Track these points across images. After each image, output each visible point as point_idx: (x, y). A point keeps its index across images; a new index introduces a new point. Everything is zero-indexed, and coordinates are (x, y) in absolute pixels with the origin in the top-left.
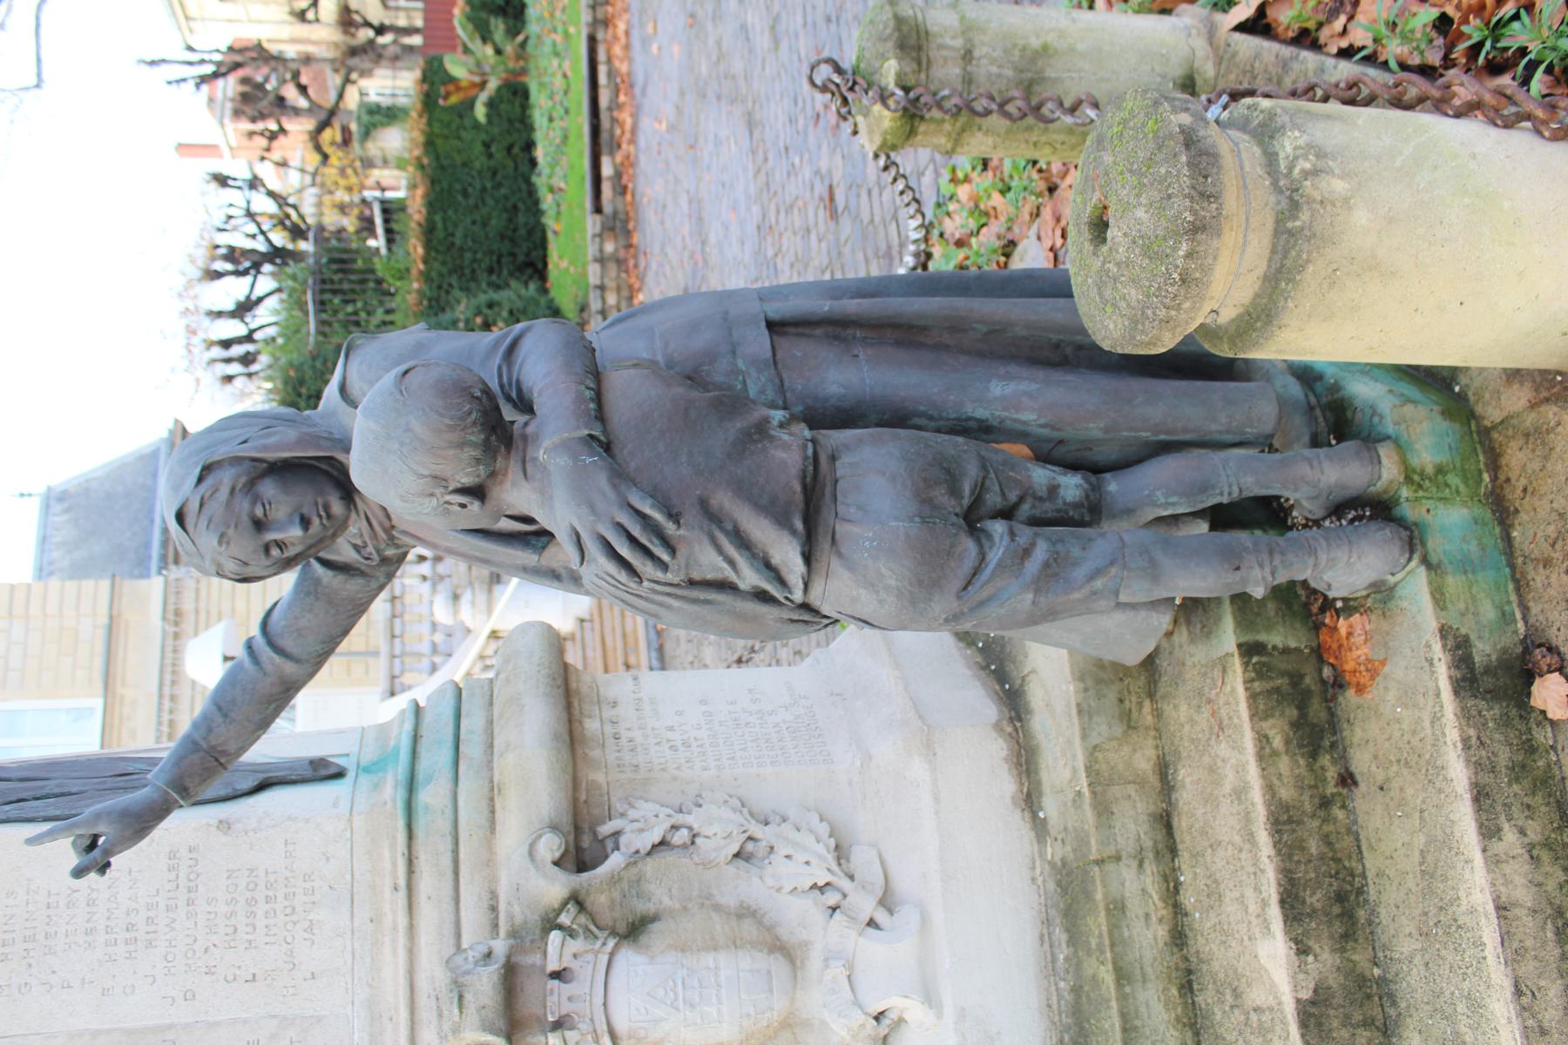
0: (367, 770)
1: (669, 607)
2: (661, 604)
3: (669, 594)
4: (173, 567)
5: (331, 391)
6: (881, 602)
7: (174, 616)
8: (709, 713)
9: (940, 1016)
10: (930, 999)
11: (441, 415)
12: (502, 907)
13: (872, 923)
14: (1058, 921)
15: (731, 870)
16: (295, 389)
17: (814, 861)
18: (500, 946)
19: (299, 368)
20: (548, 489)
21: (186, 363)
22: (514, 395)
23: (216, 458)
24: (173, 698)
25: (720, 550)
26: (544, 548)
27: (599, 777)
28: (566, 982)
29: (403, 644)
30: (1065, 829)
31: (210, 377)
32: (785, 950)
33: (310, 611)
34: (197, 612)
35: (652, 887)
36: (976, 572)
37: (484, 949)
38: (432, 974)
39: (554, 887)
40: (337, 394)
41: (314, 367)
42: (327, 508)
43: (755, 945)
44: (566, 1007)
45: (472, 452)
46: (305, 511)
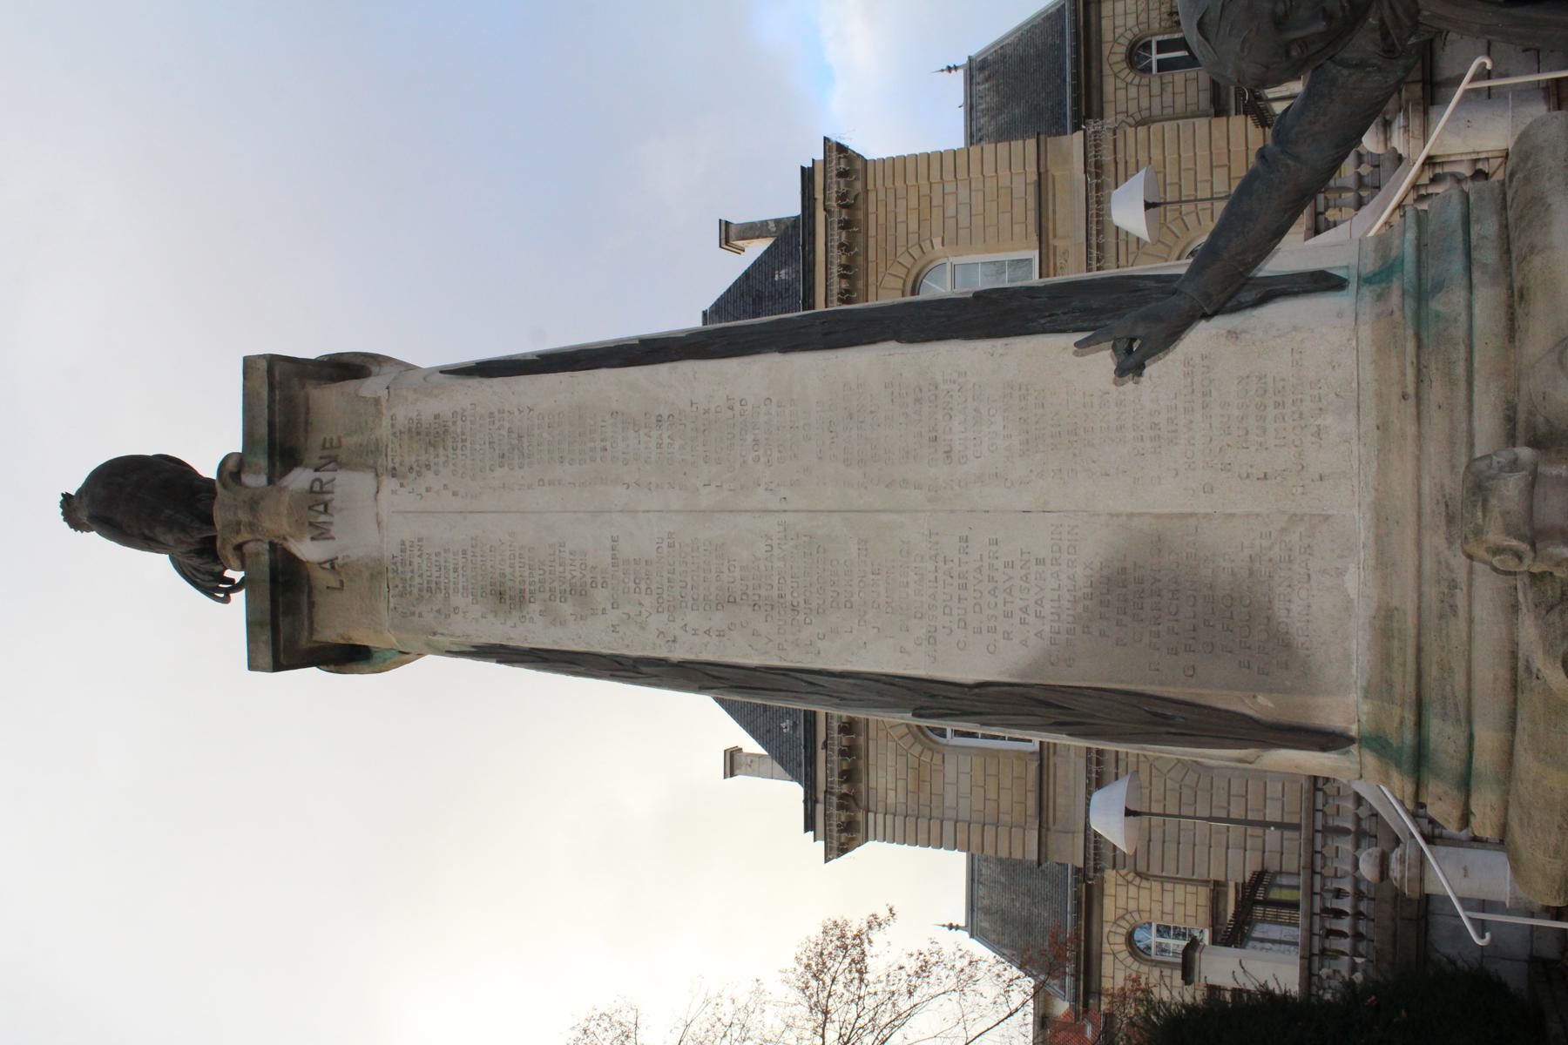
7: (1094, 168)
24: (1100, 247)
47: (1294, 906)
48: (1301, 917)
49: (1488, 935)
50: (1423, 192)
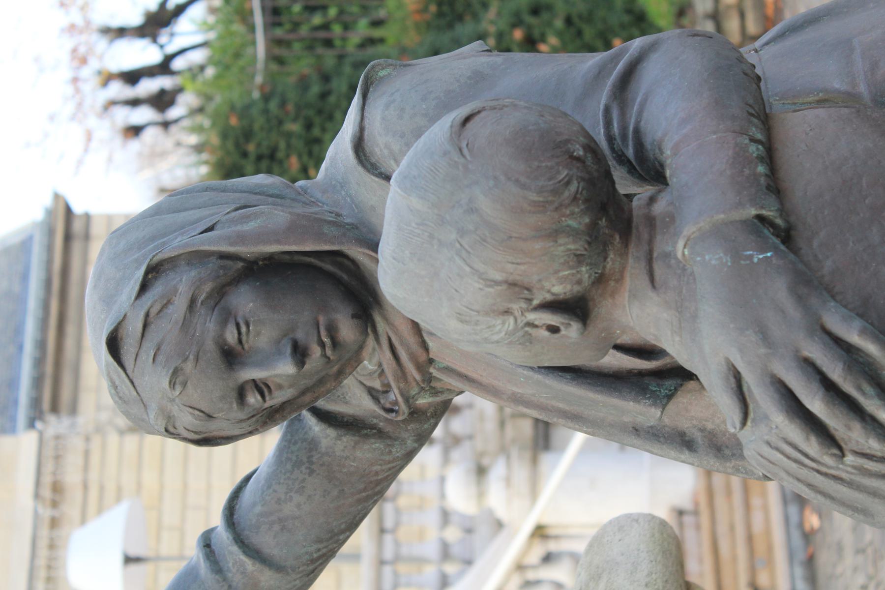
4: (51, 419)
5: (340, 148)
7: (52, 493)
11: (523, 187)
16: (237, 145)
19: (244, 112)
20: (694, 307)
21: (70, 107)
22: (630, 153)
23: (166, 254)
26: (669, 397)
29: (397, 544)
31: (106, 129)
33: (301, 490)
34: (85, 487)
40: (350, 153)
41: (266, 111)
42: (332, 330)
45: (568, 245)
46: (300, 335)
50: (531, 575)
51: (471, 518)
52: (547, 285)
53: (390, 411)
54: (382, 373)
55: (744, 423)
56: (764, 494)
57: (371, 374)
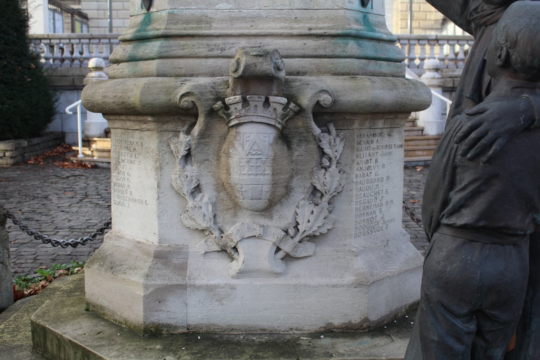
0: (365, 17)
1: (443, 157)
2: (445, 153)
3: (449, 157)
6: (438, 263)
8: (382, 179)
9: (233, 277)
10: (241, 274)
12: (299, 77)
13: (278, 249)
14: (271, 338)
15: (308, 185)
17: (310, 224)
18: (282, 74)
25: (470, 183)
27: (356, 126)
28: (264, 104)
30: (315, 347)
32: (268, 208)
35: (303, 147)
36: (451, 313)
37: (282, 67)
38: (271, 44)
39: (306, 100)
43: (273, 193)
44: (252, 104)
47: (73, 30)
48: (68, 33)
49: (71, 113)
51: (422, 68)
52: (515, 53)
53: (470, 14)
54: (483, 11)
55: (467, 114)
56: (427, 155)
57: (483, 8)
